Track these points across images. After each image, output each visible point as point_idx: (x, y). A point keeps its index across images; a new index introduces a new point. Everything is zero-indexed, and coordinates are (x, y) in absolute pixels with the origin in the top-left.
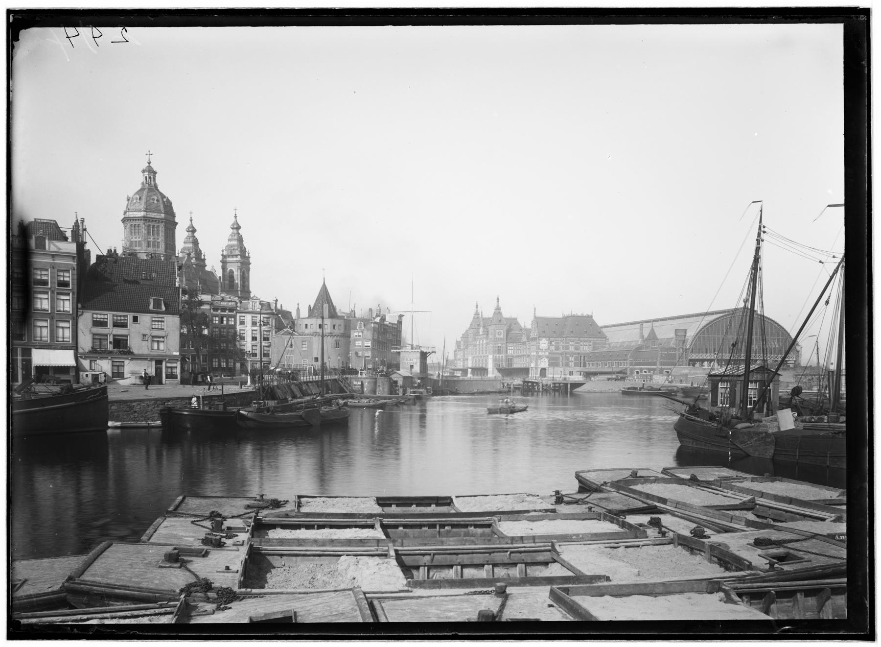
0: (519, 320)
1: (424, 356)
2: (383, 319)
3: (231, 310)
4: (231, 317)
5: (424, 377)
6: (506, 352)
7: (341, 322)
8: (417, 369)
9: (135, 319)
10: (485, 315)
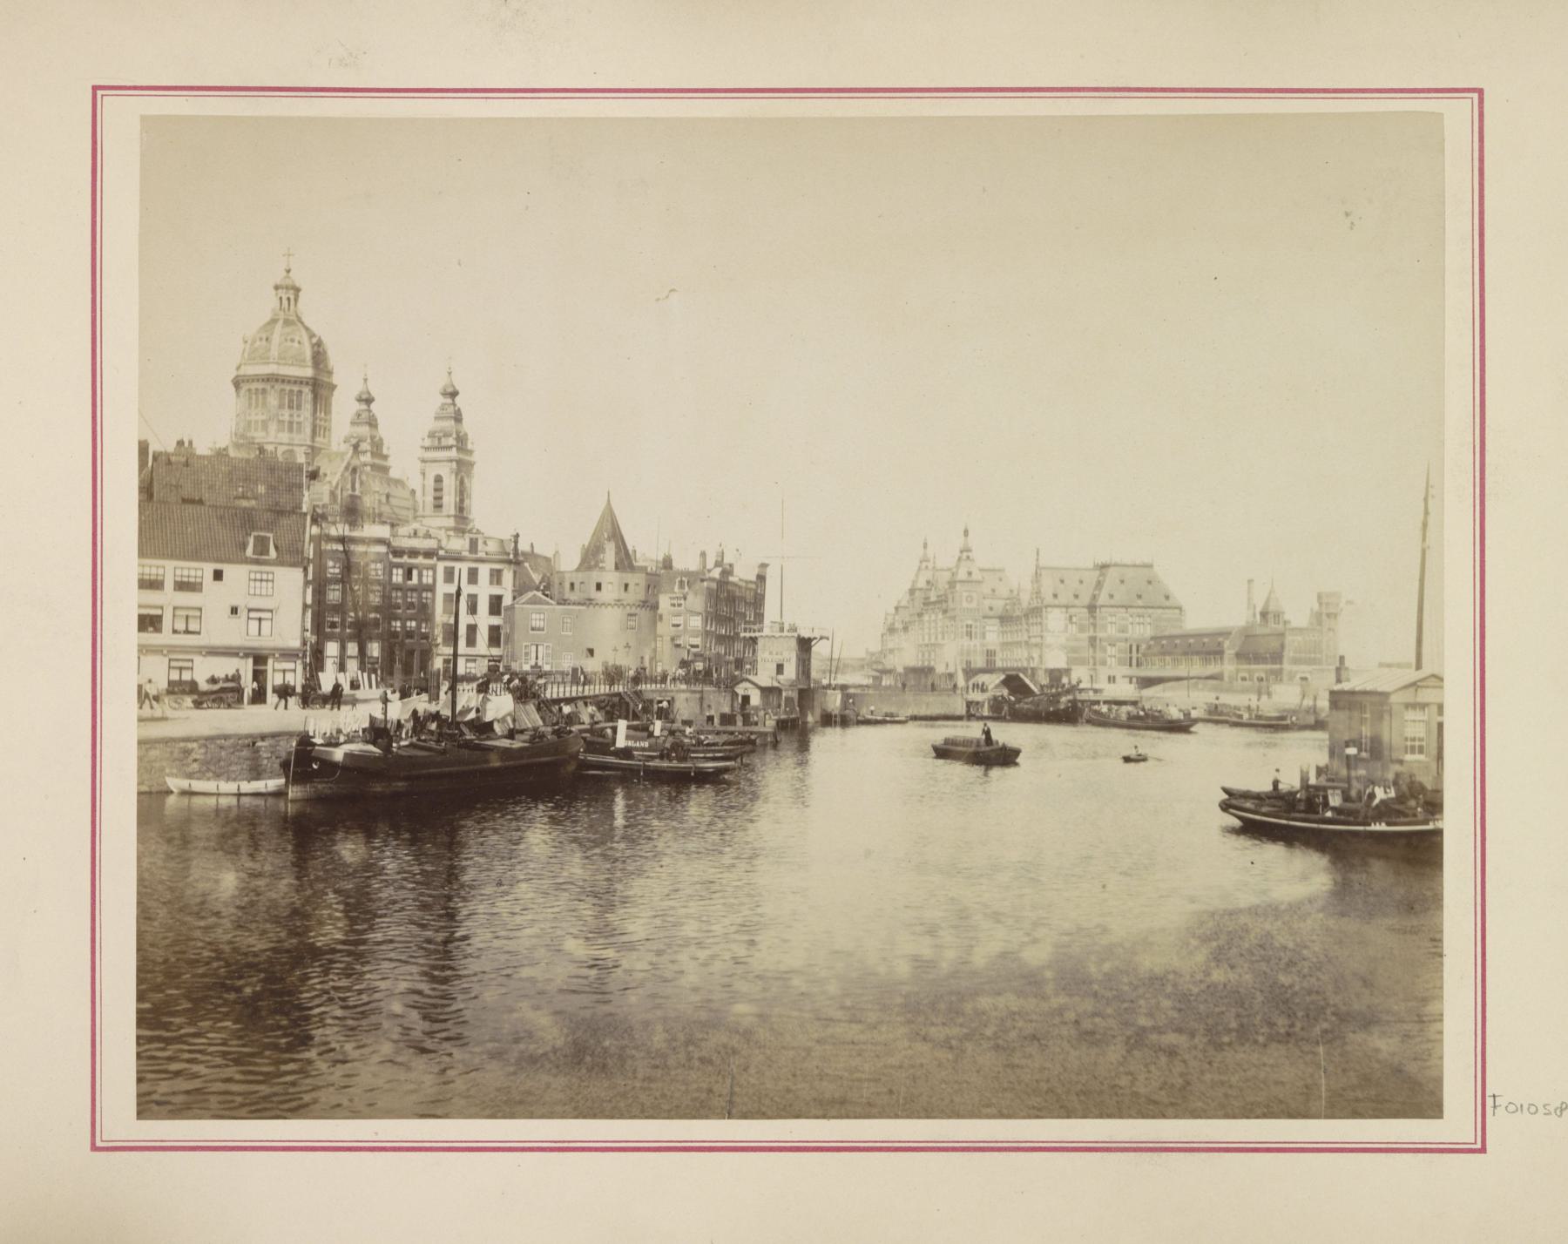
0: (336, 393)
1: (805, 645)
2: (727, 572)
3: (429, 554)
8: (791, 672)
9: (218, 575)
10: (199, 452)
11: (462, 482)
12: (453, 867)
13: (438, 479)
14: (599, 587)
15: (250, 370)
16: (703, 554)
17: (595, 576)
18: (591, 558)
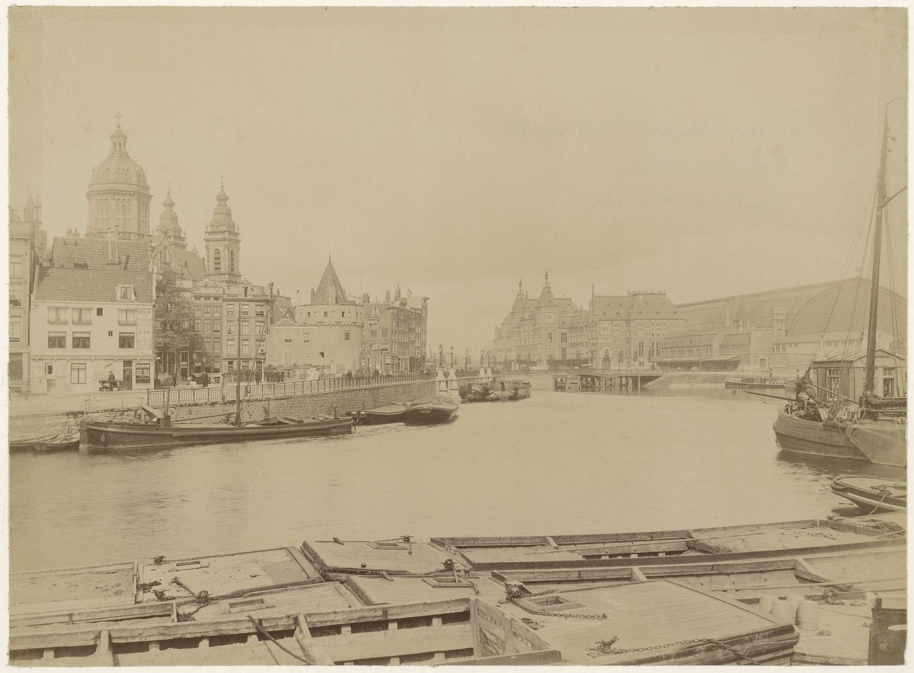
2: (404, 304)
9: (100, 312)
11: (232, 253)
12: (349, 427)
13: (217, 252)
14: (326, 314)
16: (388, 293)
18: (317, 297)
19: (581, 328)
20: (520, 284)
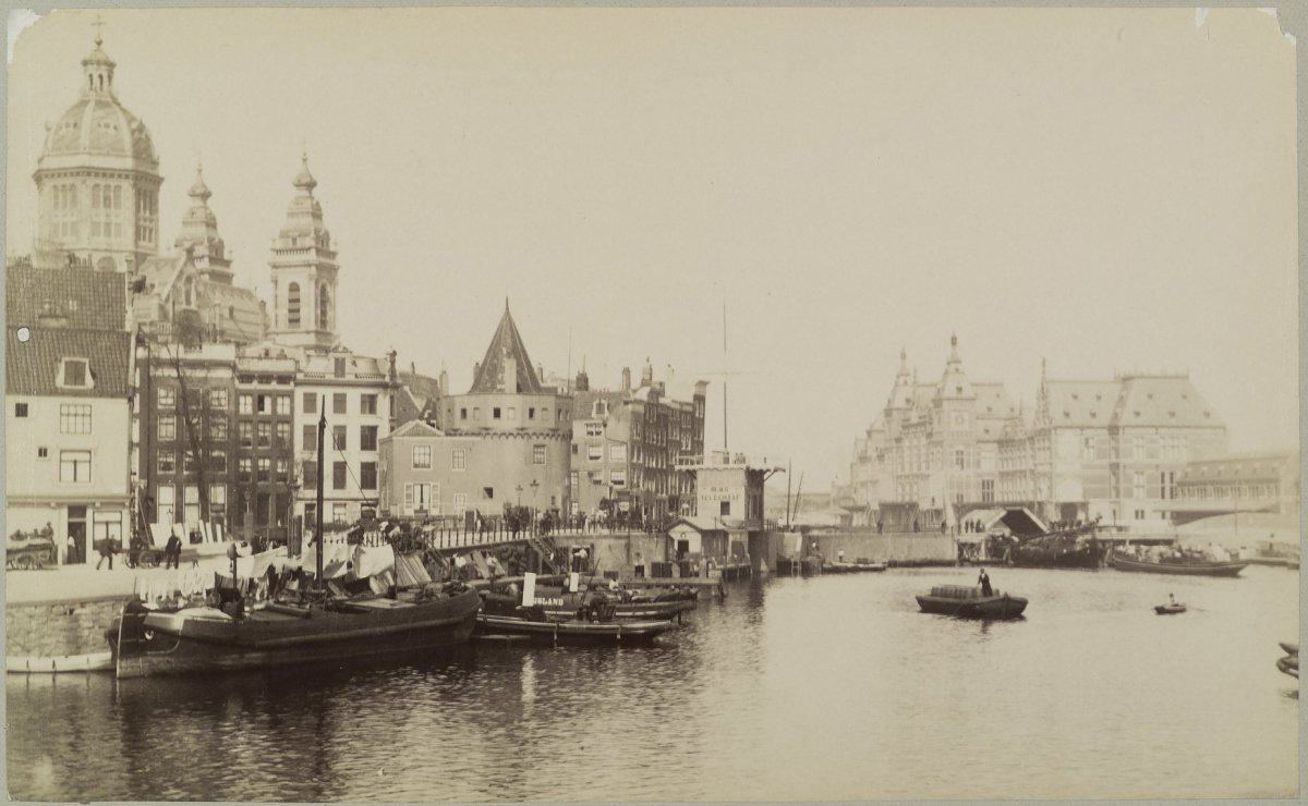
1: (755, 479)
2: (657, 393)
4: (283, 395)
5: (759, 537)
6: (978, 464)
7: (550, 402)
8: (738, 511)
11: (323, 291)
13: (294, 288)
14: (497, 413)
15: (52, 163)
16: (627, 372)
17: (492, 401)
18: (486, 377)
19: (1022, 442)
20: (903, 356)
